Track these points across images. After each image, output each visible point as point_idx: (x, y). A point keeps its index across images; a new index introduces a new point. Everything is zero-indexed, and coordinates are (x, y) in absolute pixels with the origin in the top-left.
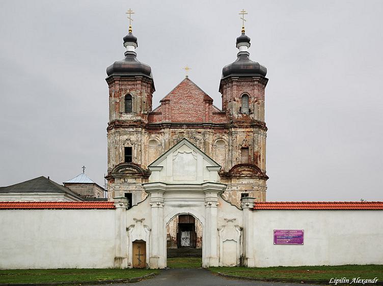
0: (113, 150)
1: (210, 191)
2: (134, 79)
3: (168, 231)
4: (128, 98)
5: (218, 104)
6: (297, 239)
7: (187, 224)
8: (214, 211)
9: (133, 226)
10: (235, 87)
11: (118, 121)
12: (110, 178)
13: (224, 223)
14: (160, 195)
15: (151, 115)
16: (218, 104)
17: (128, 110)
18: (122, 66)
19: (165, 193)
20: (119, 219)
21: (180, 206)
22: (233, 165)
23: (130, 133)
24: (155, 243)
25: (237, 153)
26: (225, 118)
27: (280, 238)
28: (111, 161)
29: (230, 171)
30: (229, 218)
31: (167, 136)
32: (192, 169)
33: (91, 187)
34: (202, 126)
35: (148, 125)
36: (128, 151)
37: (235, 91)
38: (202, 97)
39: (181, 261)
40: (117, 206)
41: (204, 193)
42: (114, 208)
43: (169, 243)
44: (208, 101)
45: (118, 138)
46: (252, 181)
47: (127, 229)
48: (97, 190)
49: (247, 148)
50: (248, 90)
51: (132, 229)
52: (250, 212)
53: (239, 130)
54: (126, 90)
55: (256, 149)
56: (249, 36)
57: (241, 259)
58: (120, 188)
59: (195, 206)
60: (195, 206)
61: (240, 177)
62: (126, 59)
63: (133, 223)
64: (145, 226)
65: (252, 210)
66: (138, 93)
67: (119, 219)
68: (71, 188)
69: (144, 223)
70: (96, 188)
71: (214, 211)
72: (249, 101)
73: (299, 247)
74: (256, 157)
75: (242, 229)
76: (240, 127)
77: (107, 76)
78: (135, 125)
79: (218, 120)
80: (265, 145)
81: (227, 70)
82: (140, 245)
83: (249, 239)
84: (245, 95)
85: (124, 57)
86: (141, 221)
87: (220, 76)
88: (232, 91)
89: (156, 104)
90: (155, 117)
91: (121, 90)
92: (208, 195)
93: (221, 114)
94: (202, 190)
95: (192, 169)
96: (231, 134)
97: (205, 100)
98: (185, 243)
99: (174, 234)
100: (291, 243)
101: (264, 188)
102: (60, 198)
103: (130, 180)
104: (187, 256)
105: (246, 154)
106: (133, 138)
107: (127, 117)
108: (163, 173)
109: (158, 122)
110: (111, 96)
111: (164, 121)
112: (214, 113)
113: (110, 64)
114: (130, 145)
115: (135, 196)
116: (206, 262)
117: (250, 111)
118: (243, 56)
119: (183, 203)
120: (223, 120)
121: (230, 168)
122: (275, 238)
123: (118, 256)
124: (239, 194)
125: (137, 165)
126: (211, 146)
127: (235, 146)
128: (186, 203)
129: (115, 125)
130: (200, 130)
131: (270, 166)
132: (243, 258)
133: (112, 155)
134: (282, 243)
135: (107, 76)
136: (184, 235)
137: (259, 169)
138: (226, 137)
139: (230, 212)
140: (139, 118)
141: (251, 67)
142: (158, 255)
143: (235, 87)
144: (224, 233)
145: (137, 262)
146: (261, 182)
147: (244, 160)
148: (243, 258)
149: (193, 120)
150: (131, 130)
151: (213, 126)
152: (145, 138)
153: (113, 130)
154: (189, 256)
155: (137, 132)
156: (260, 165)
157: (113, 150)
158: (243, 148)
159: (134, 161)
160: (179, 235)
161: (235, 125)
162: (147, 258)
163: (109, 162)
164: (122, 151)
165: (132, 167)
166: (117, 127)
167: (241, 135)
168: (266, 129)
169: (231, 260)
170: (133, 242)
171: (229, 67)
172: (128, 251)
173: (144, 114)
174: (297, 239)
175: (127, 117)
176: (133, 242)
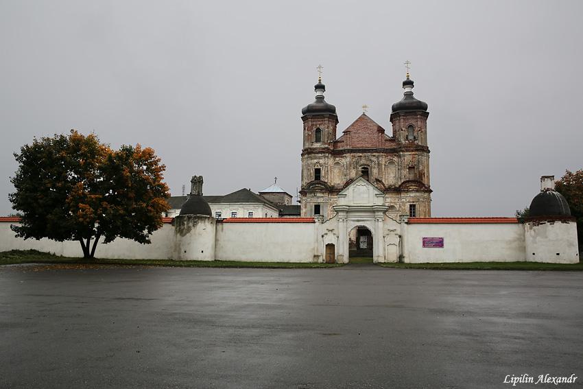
0: (305, 171)
1: (378, 211)
2: (323, 117)
3: (349, 235)
4: (318, 131)
5: (389, 132)
6: (439, 243)
7: (363, 232)
8: (380, 224)
9: (326, 234)
10: (402, 120)
11: (310, 149)
12: (303, 192)
13: (388, 232)
14: (345, 214)
15: (336, 142)
16: (389, 132)
17: (318, 140)
18: (314, 108)
19: (347, 212)
20: (317, 229)
21: (358, 221)
22: (402, 181)
23: (319, 158)
24: (341, 246)
25: (405, 172)
26: (395, 144)
27: (427, 243)
28: (304, 179)
29: (400, 186)
30: (391, 229)
31: (348, 159)
32: (366, 196)
33: (282, 195)
34: (376, 151)
35: (333, 151)
36: (318, 171)
37: (402, 123)
38: (376, 128)
39: (359, 260)
40: (316, 220)
41: (374, 212)
42: (314, 222)
43: (351, 245)
44: (381, 130)
45: (310, 162)
46: (418, 194)
47: (323, 236)
48: (286, 198)
49: (414, 168)
50: (412, 122)
51: (325, 236)
52: (406, 225)
53: (406, 153)
54: (316, 125)
55: (421, 168)
56: (412, 80)
57: (400, 257)
58: (311, 201)
59: (368, 220)
60: (368, 220)
61: (408, 191)
62: (316, 102)
63: (327, 232)
64: (334, 234)
65: (407, 223)
66: (325, 127)
67: (317, 229)
68: (266, 196)
69: (334, 232)
70: (286, 196)
71: (380, 224)
72: (414, 130)
73: (441, 249)
74: (421, 175)
75: (400, 237)
76: (407, 151)
77: (302, 115)
78: (324, 151)
79: (389, 145)
80: (428, 165)
81: (395, 107)
82: (330, 247)
83: (405, 244)
84: (411, 126)
85: (315, 100)
86: (331, 231)
87: (390, 112)
88: (399, 122)
89: (339, 134)
90: (339, 144)
91: (312, 125)
92: (377, 214)
93: (393, 140)
94: (372, 210)
95: (366, 196)
96: (399, 157)
97: (378, 130)
98: (363, 246)
99: (354, 238)
100: (435, 246)
101: (429, 200)
102: (259, 212)
103: (319, 195)
104: (363, 256)
105: (413, 172)
106: (322, 161)
107: (317, 145)
108: (346, 199)
109: (341, 149)
110: (305, 129)
111: (346, 148)
112: (387, 140)
113: (305, 105)
114: (319, 167)
115: (323, 207)
116: (375, 259)
117: (415, 138)
118: (409, 95)
119: (359, 219)
120: (393, 145)
121: (400, 183)
122: (424, 242)
123: (316, 254)
124: (408, 205)
125: (325, 182)
126: (383, 166)
127: (403, 165)
128: (362, 219)
129: (307, 152)
130: (374, 154)
131: (434, 181)
132: (401, 257)
133: (305, 175)
134: (428, 246)
135: (302, 115)
136: (362, 239)
137: (424, 185)
138: (395, 159)
139: (392, 225)
140: (327, 146)
141: (415, 105)
142: (343, 252)
143: (402, 120)
144: (388, 239)
145: (328, 259)
146: (426, 195)
147: (411, 177)
148: (401, 257)
149: (369, 146)
150: (320, 155)
151: (386, 151)
152: (331, 161)
153: (306, 156)
154: (366, 256)
155: (325, 157)
156: (425, 181)
157: (305, 171)
158: (410, 168)
159: (322, 179)
160: (358, 239)
161: (403, 149)
162: (336, 256)
163: (302, 180)
164: (312, 171)
165: (321, 184)
166: (309, 153)
167: (408, 157)
168: (429, 152)
169: (393, 258)
170: (326, 245)
171: (397, 105)
172: (323, 251)
173: (330, 142)
174: (439, 243)
175: (317, 145)
176: (326, 245)
